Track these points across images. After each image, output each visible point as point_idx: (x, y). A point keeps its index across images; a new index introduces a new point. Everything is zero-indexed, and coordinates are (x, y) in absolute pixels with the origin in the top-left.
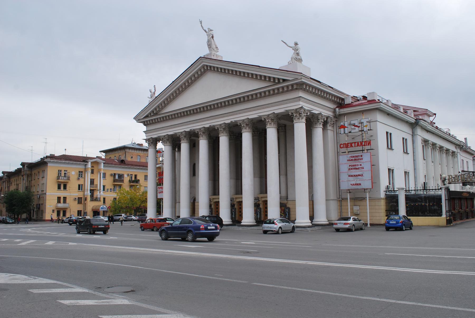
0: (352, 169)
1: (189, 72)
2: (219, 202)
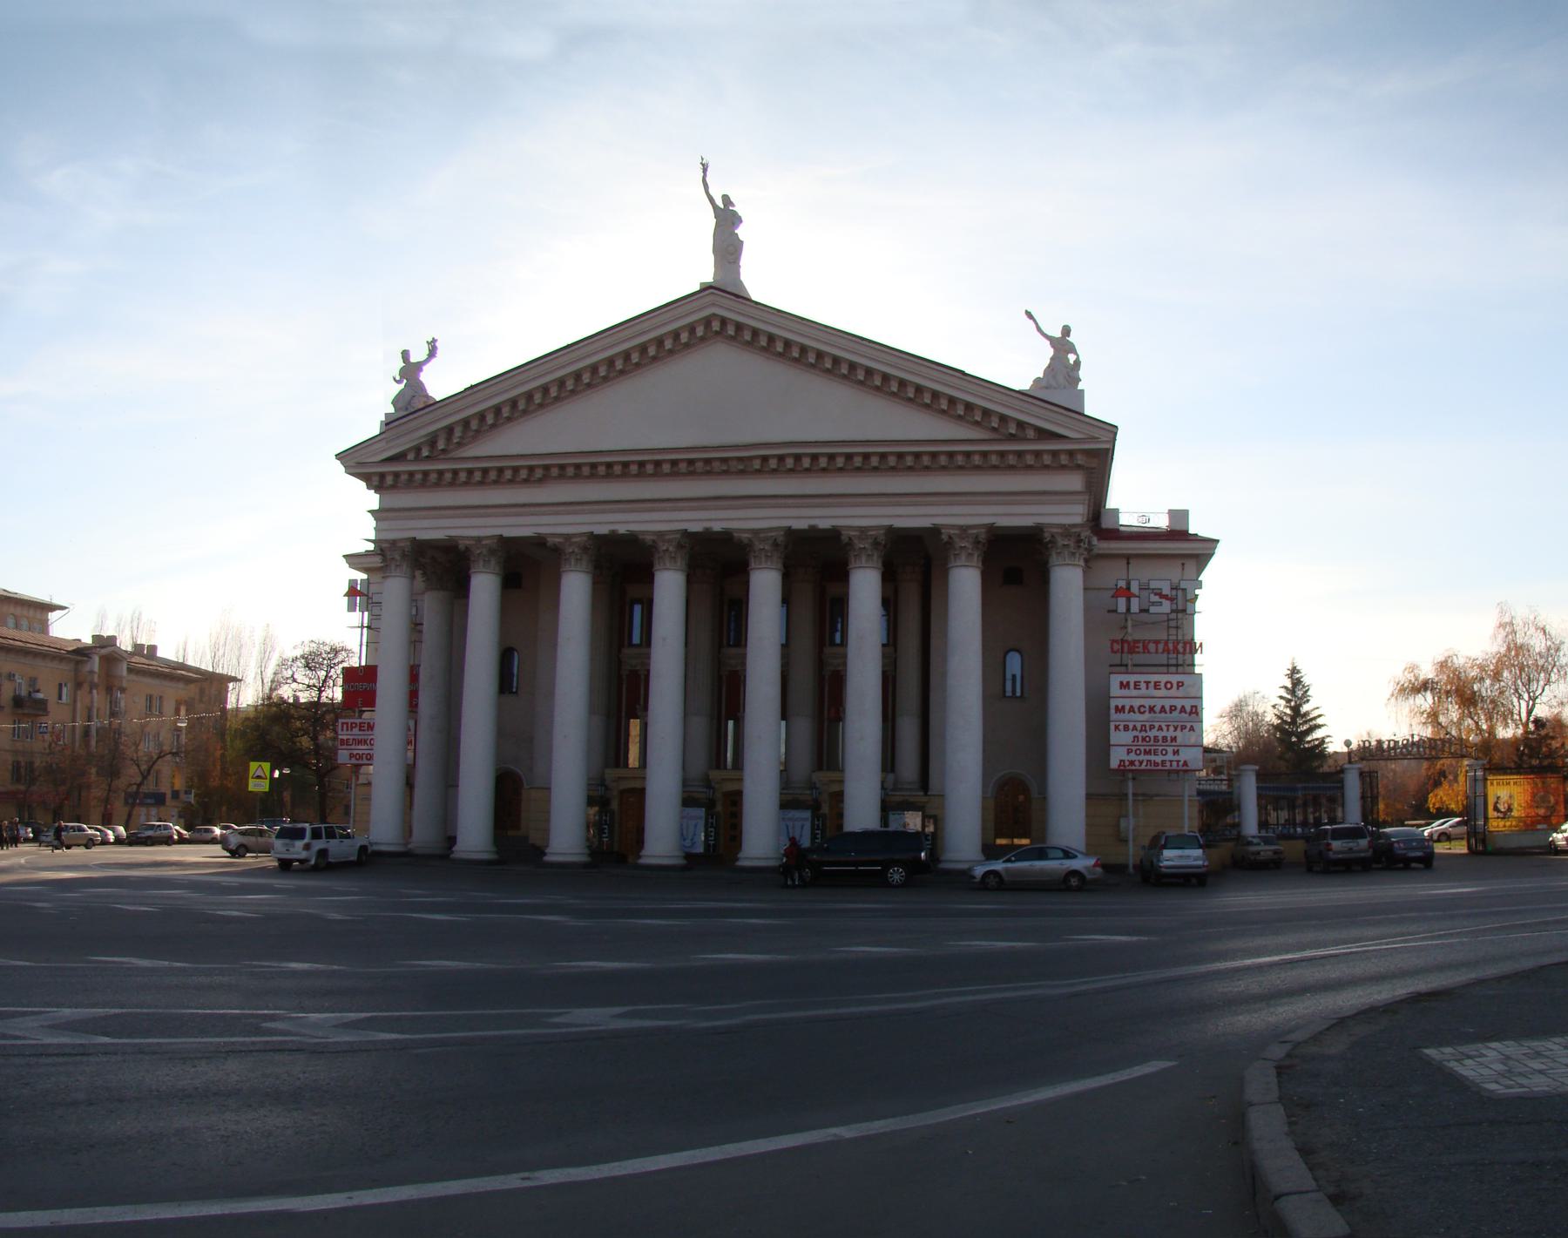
1: (646, 326)
2: (739, 793)
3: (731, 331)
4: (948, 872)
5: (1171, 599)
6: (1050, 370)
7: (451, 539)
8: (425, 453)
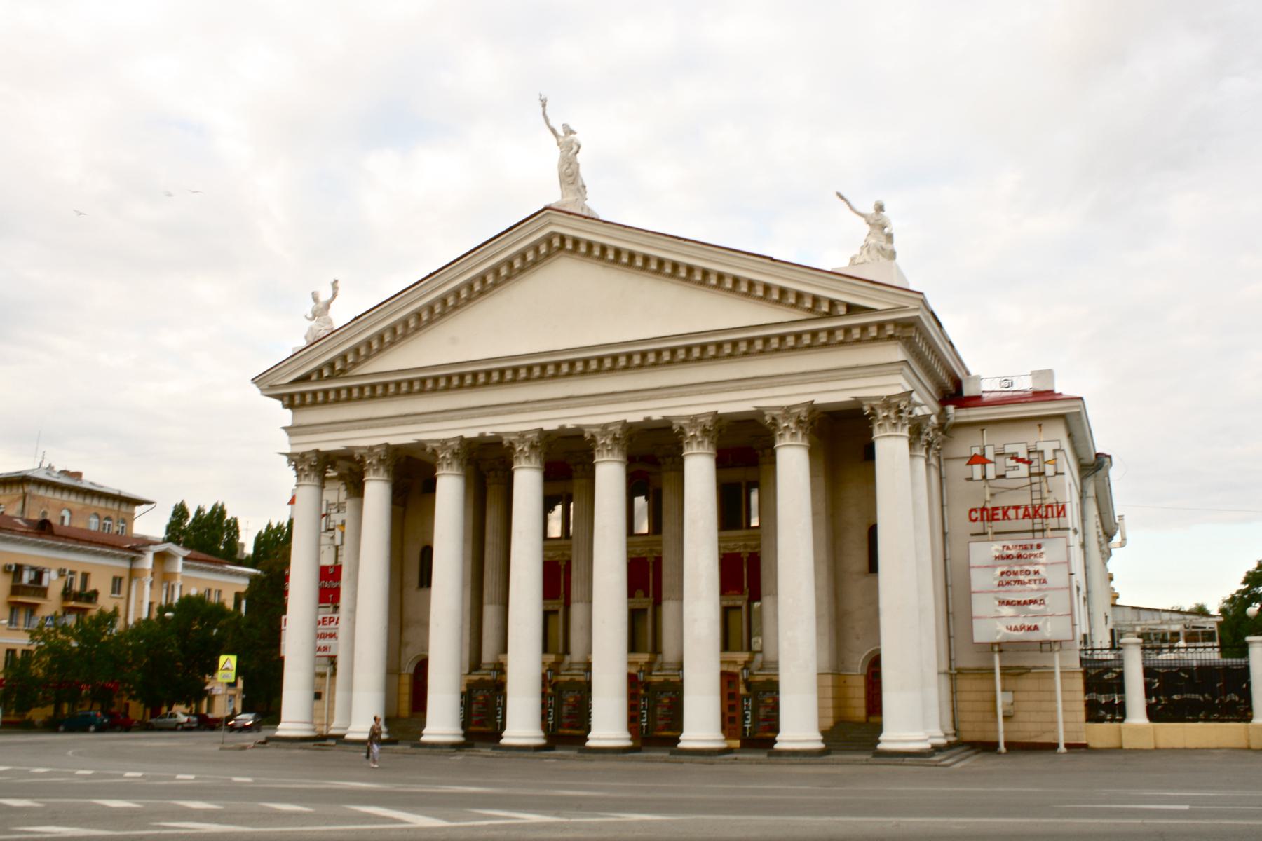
0: (1008, 583)
3: (569, 246)
5: (1029, 463)
7: (858, 400)
8: (326, 373)
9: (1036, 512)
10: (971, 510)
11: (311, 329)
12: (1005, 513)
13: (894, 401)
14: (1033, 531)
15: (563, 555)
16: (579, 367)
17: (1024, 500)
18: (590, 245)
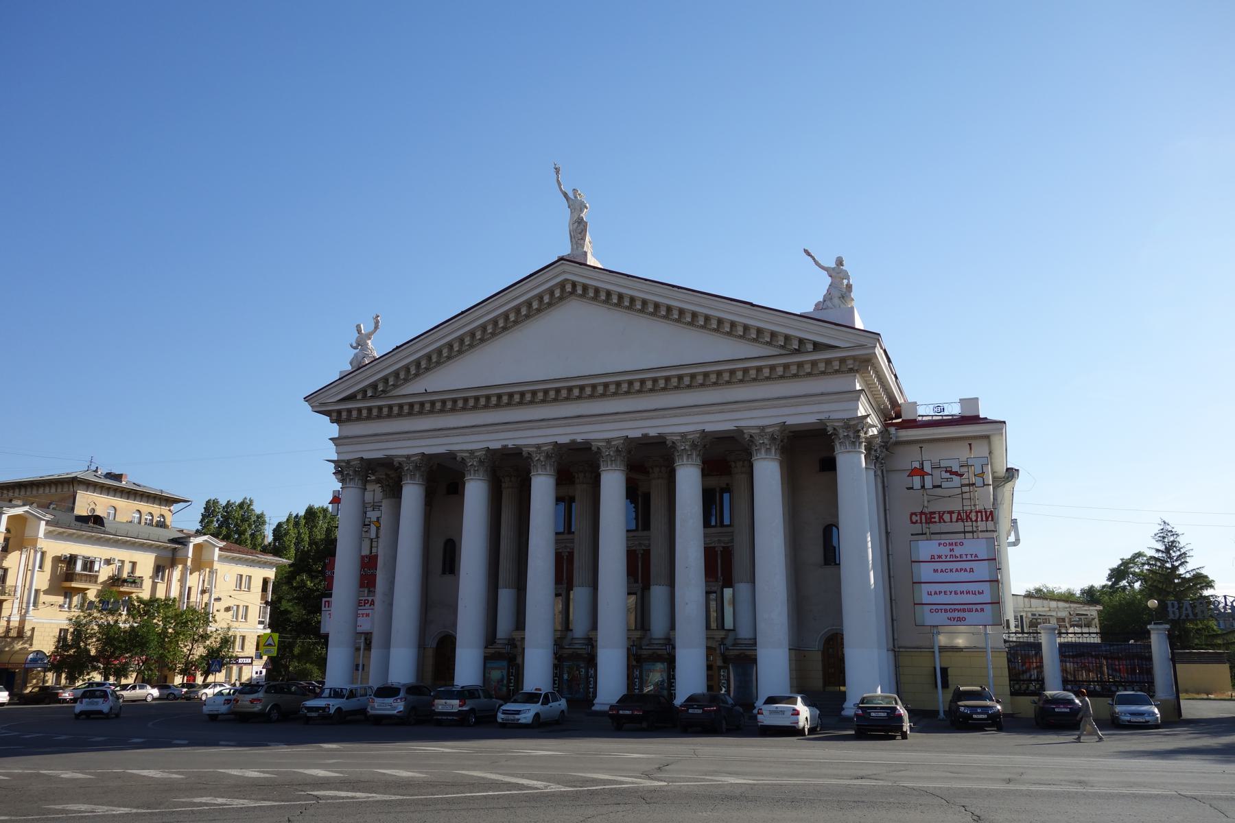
3: (580, 291)
4: (710, 688)
6: (828, 297)
8: (369, 393)
9: (968, 516)
10: (912, 514)
11: (356, 355)
12: (941, 518)
13: (852, 423)
14: (965, 532)
15: (640, 544)
16: (588, 391)
17: (956, 506)
18: (597, 290)
